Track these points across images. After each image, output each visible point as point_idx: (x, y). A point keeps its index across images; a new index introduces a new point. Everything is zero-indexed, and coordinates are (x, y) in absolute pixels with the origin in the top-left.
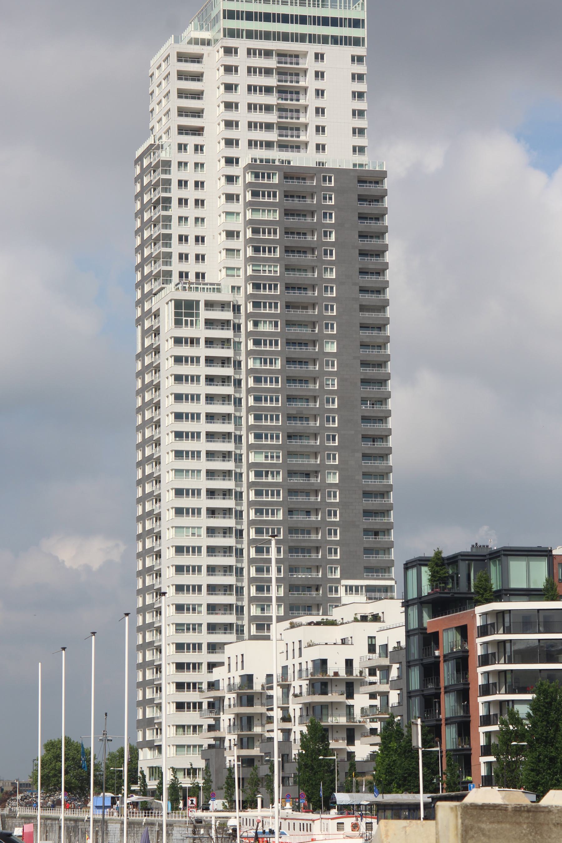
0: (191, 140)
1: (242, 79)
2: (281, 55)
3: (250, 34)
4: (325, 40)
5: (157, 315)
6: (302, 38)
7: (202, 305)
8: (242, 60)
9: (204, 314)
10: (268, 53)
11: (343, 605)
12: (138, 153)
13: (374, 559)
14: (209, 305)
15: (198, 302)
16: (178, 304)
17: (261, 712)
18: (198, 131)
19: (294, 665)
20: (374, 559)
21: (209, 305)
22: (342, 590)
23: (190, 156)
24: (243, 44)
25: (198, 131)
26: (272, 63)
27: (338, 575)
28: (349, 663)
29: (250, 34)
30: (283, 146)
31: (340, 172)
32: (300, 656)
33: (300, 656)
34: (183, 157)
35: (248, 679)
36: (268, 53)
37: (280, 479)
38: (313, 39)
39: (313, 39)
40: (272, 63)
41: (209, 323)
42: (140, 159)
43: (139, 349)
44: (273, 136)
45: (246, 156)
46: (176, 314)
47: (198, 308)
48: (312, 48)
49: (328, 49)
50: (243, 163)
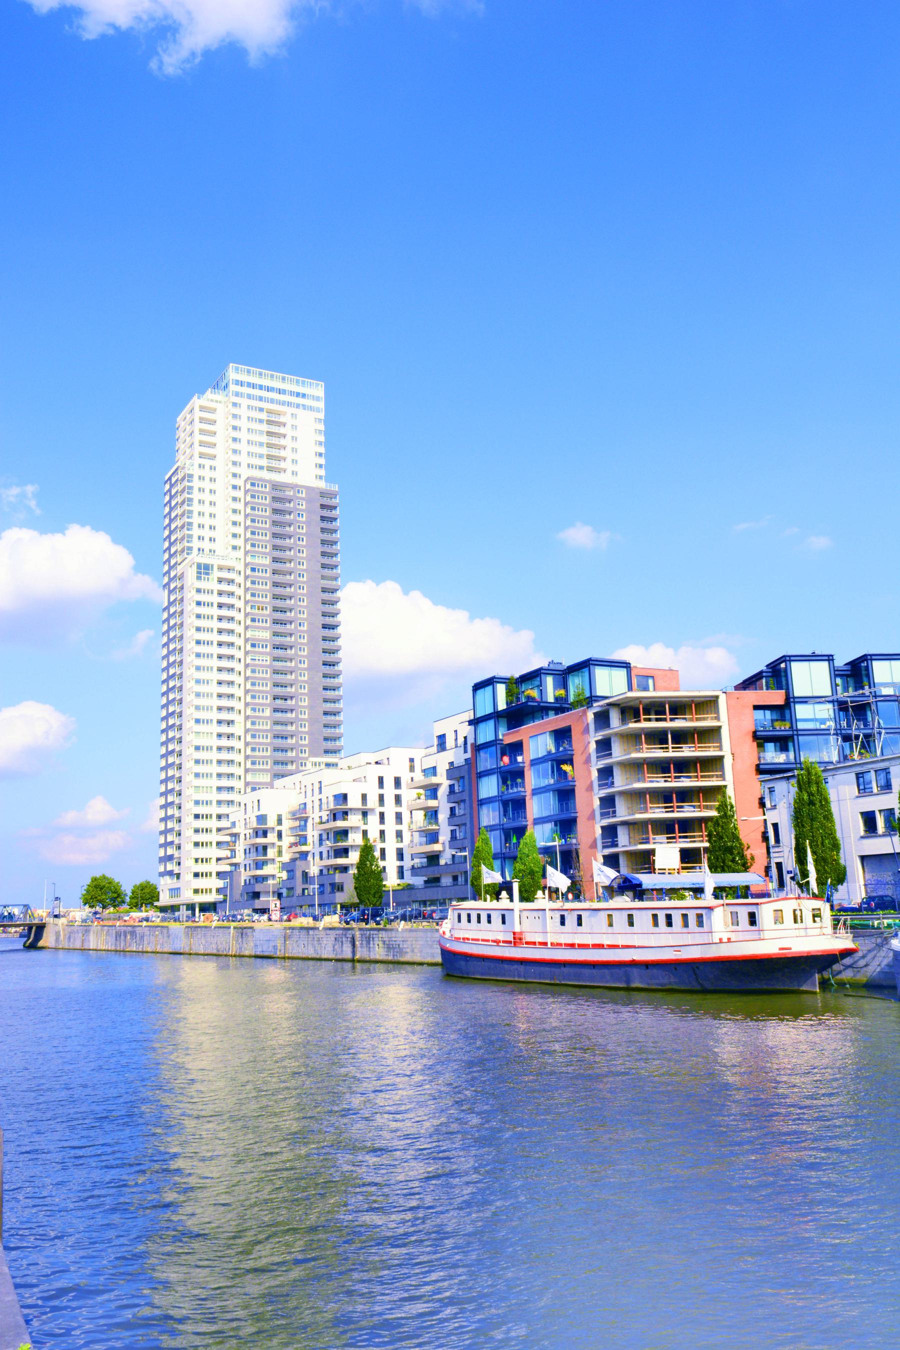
0: (207, 463)
1: (243, 447)
2: (269, 412)
3: (249, 397)
4: (298, 406)
5: (181, 577)
6: (283, 403)
7: (215, 568)
8: (243, 412)
9: (216, 574)
10: (261, 410)
11: (42, 948)
12: (167, 477)
13: (330, 745)
14: (221, 568)
15: (212, 566)
16: (199, 566)
17: (893, 784)
18: (213, 457)
19: (456, 731)
20: (330, 745)
21: (221, 568)
22: (309, 765)
23: (207, 473)
24: (244, 402)
25: (213, 457)
26: (264, 416)
27: (307, 755)
28: (364, 797)
29: (249, 397)
30: (270, 469)
31: (308, 488)
32: (321, 793)
33: (321, 793)
34: (202, 472)
35: (262, 819)
36: (261, 410)
37: (268, 688)
38: (289, 404)
39: (289, 404)
40: (264, 416)
41: (220, 581)
42: (170, 479)
43: (166, 604)
44: (264, 462)
45: (245, 473)
46: (198, 573)
47: (212, 570)
48: (290, 410)
49: (300, 412)
50: (244, 478)
